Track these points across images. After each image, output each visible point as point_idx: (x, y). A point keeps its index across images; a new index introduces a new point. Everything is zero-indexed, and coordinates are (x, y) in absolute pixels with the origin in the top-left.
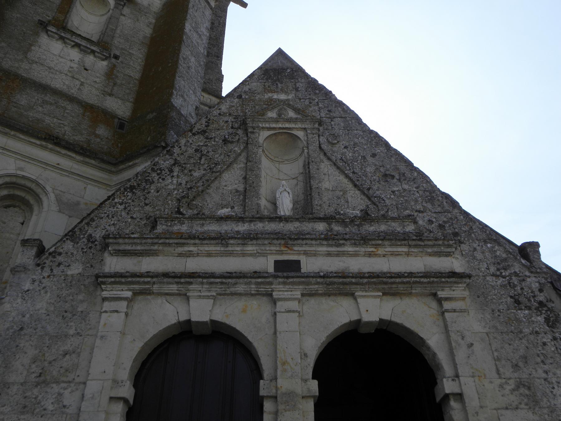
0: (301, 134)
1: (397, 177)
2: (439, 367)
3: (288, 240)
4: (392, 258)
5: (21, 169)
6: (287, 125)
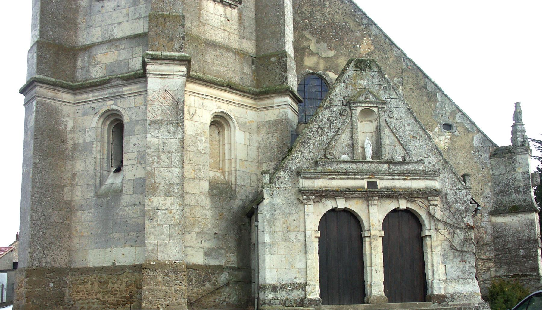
0: (375, 110)
1: (418, 138)
2: (424, 225)
3: (373, 174)
4: (413, 181)
5: (219, 107)
6: (370, 105)
